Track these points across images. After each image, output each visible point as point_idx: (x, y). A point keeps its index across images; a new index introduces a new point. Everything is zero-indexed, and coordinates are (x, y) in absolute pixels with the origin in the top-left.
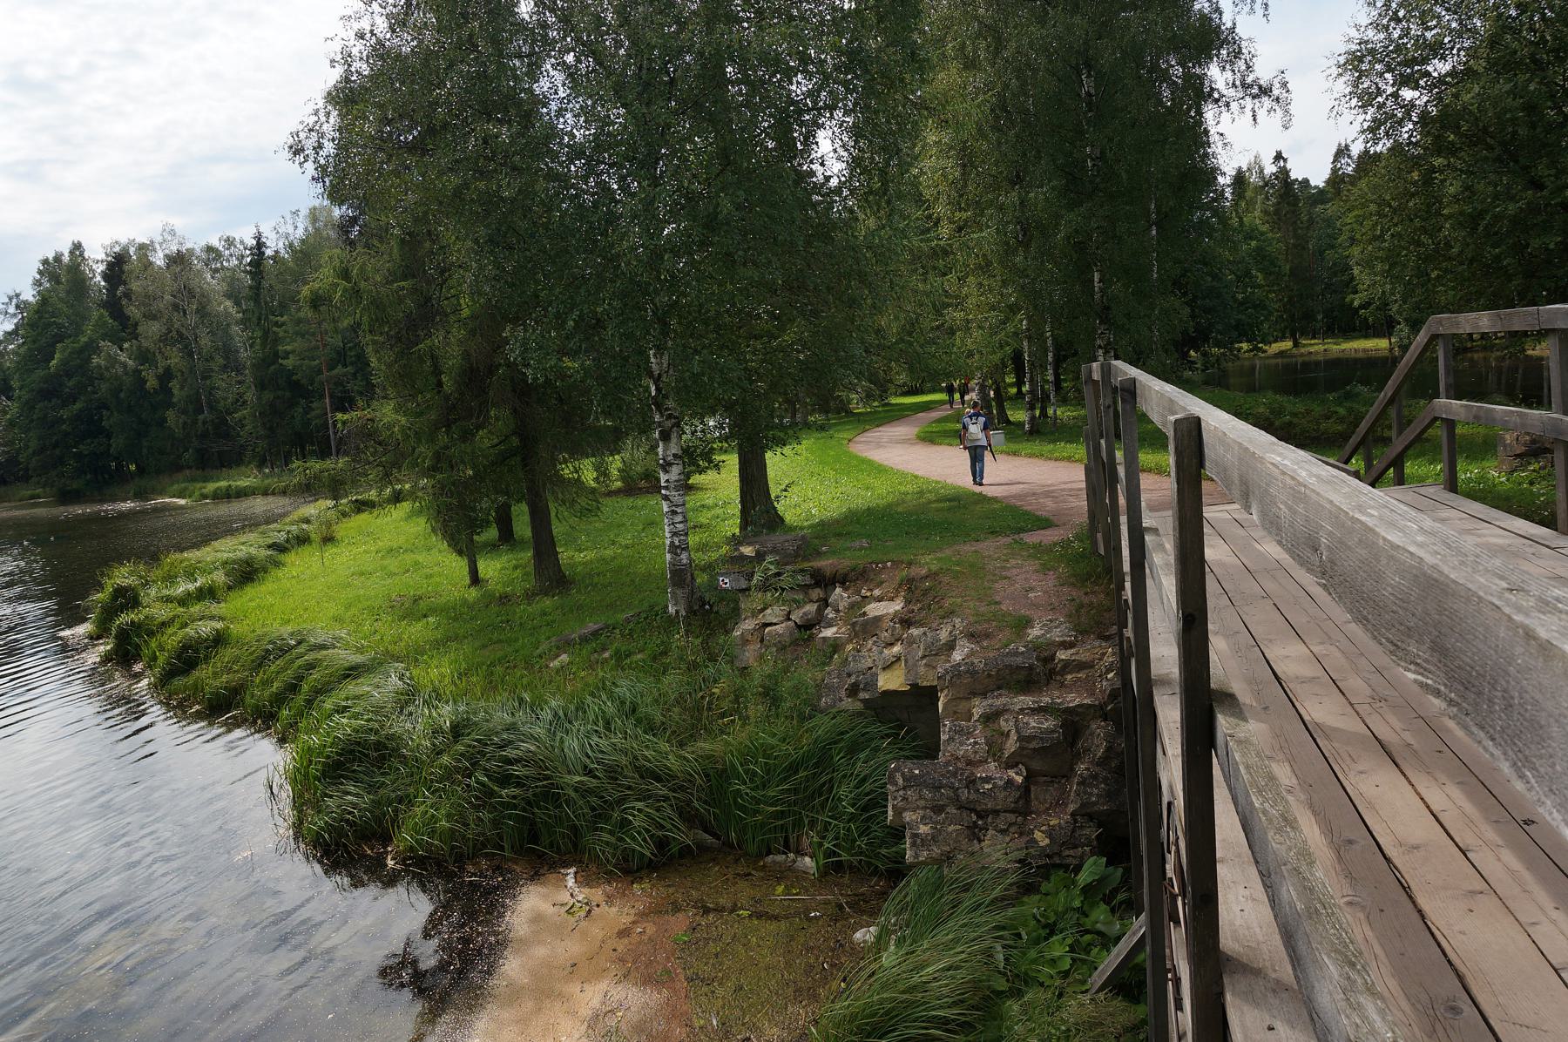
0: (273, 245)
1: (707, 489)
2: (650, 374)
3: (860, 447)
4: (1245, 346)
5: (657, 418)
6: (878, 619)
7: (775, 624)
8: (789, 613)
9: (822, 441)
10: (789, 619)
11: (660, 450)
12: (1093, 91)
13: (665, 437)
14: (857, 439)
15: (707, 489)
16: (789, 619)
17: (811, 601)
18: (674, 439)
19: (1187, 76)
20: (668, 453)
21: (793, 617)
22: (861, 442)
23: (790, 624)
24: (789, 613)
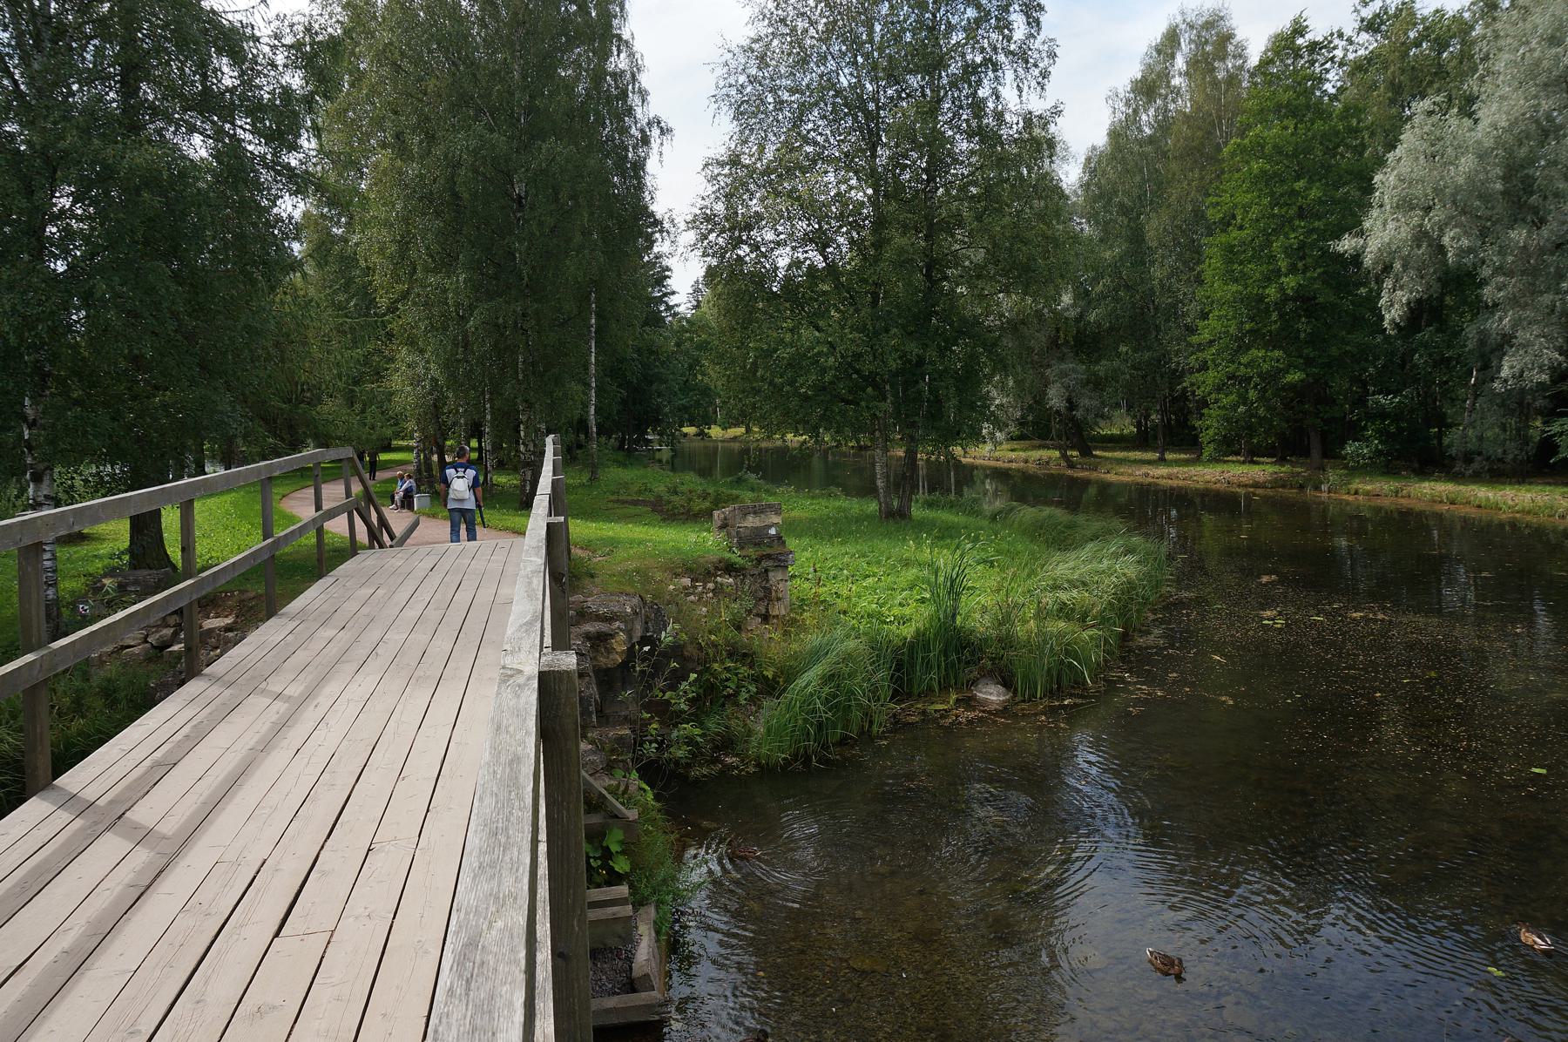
0: (1484, 518)
1: (104, 540)
2: (24, 418)
3: (292, 503)
4: (690, 430)
5: (29, 460)
6: (211, 630)
7: (133, 646)
8: (147, 636)
9: (251, 495)
10: (147, 642)
11: (31, 491)
12: (523, 194)
13: (37, 479)
14: (293, 495)
15: (104, 540)
16: (147, 642)
17: (169, 626)
18: (46, 481)
19: (242, 200)
20: (39, 493)
21: (149, 640)
22: (295, 499)
23: (147, 645)
24: (147, 636)
